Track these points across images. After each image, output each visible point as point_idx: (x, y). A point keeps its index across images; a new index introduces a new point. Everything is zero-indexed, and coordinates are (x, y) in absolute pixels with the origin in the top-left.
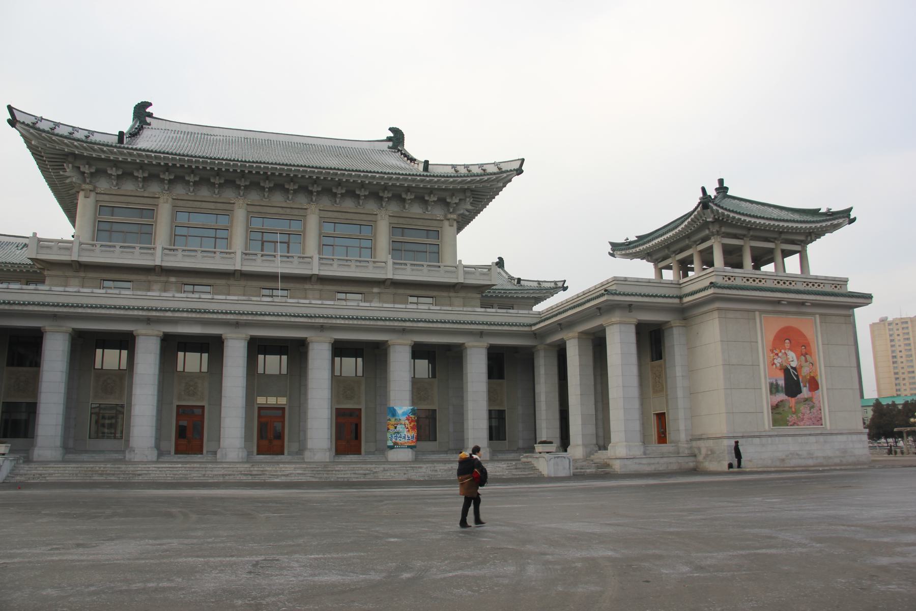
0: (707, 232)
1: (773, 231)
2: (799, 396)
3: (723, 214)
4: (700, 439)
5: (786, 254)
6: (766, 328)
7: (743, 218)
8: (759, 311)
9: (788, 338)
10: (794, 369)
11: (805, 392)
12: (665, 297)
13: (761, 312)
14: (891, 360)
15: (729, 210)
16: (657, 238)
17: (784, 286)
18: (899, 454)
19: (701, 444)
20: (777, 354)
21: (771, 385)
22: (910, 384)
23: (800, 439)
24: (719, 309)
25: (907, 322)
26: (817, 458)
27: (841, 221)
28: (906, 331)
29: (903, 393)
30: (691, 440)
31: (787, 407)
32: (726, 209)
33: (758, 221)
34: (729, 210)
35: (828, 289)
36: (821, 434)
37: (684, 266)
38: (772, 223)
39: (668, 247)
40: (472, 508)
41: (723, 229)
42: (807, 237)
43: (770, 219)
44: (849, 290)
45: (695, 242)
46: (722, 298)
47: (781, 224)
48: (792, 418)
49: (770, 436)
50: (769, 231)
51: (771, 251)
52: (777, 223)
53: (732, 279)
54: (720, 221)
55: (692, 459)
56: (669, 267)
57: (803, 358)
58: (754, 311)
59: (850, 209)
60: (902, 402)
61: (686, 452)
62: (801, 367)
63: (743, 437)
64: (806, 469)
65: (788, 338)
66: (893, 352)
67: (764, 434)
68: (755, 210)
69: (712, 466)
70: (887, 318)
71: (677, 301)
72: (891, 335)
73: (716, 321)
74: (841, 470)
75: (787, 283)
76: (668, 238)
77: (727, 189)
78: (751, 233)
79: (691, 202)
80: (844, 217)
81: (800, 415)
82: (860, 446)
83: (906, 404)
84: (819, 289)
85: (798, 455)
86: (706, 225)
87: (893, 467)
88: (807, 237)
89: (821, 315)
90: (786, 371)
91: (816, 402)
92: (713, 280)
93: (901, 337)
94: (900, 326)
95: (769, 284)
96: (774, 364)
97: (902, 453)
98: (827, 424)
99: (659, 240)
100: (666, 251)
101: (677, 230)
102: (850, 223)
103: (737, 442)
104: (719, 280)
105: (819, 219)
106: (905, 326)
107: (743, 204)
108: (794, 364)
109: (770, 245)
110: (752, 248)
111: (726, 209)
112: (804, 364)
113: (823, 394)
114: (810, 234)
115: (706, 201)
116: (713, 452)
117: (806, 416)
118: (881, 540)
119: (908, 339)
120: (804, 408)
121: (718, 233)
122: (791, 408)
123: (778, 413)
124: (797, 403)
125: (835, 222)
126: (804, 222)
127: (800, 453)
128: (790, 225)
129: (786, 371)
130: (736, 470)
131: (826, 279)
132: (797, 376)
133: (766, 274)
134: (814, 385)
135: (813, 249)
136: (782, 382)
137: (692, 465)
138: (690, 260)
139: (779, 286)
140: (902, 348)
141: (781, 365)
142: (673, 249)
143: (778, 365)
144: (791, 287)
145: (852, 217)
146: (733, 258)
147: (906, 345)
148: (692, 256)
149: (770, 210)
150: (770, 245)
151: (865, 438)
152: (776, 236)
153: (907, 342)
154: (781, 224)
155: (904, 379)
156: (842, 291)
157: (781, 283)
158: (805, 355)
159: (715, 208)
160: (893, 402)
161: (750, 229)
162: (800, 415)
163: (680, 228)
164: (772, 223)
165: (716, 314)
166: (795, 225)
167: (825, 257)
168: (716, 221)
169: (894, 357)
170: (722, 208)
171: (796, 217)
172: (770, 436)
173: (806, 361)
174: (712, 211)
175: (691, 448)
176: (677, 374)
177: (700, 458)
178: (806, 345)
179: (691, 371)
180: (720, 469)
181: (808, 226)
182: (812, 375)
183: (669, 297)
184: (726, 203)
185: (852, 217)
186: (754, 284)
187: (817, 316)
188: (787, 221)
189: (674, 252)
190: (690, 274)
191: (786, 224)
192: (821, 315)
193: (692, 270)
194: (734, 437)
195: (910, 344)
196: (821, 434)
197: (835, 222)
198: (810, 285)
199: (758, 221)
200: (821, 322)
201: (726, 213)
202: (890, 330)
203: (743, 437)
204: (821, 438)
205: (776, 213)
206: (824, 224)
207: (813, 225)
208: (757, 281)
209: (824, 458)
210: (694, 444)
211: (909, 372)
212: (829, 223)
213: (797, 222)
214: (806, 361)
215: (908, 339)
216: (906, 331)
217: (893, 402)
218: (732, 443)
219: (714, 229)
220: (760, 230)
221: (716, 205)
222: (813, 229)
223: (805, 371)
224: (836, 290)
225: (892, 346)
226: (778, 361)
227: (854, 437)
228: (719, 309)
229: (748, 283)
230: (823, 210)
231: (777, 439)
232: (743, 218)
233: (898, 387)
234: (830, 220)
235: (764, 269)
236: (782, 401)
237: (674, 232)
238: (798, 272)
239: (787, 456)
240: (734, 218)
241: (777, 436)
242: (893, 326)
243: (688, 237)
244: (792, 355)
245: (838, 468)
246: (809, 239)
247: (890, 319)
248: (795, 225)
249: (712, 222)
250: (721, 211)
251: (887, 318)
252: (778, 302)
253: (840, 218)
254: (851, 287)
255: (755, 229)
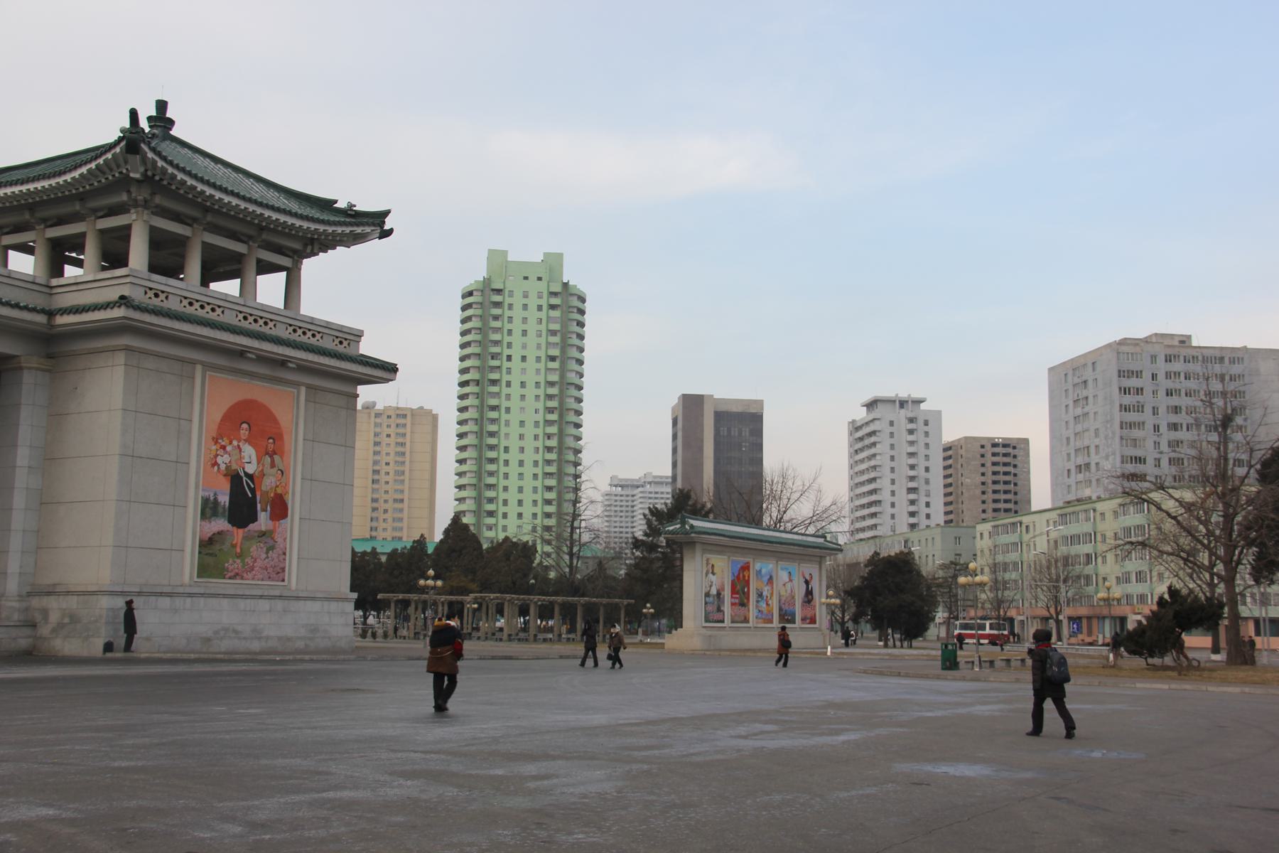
0: (124, 197)
1: (251, 223)
2: (251, 526)
3: (164, 171)
4: (49, 594)
5: (266, 268)
6: (212, 396)
7: (200, 187)
8: (202, 363)
9: (246, 420)
10: (250, 477)
11: (263, 520)
12: (17, 306)
13: (207, 367)
14: (370, 477)
15: (177, 167)
16: (16, 183)
17: (255, 327)
18: (369, 638)
19: (53, 603)
20: (224, 448)
21: (206, 501)
22: (394, 520)
23: (242, 603)
24: (127, 349)
25: (405, 416)
26: (268, 638)
27: (368, 229)
28: (401, 430)
29: (380, 534)
30: (29, 594)
31: (228, 544)
32: (171, 163)
33: (227, 199)
34: (177, 167)
35: (328, 344)
36: (280, 597)
37: (58, 255)
38: (251, 208)
39: (32, 207)
40: (1049, 705)
41: (158, 200)
42: (306, 245)
43: (250, 200)
44: (362, 351)
45: (94, 211)
46: (137, 330)
47: (267, 213)
48: (233, 565)
49: (191, 595)
50: (243, 221)
51: (239, 258)
52: (259, 210)
53: (162, 296)
54: (155, 182)
55: (27, 631)
56: (26, 249)
57: (268, 459)
58: (193, 363)
59: (387, 213)
60: (389, 550)
61: (16, 616)
62: (263, 475)
63: (140, 594)
64: (252, 657)
65: (246, 420)
66: (375, 463)
67: (181, 590)
68: (219, 173)
69: (68, 646)
70: (374, 404)
71: (41, 319)
72: (376, 435)
73: (119, 372)
74: (311, 661)
75: (261, 322)
76: (44, 190)
77: (171, 122)
78: (209, 218)
79: (108, 130)
80: (373, 224)
81: (248, 560)
82: (340, 620)
83: (393, 555)
84: (313, 341)
85: (235, 631)
86: (125, 182)
87: (393, 659)
88: (306, 245)
89: (309, 387)
90: (235, 479)
91: (279, 540)
92: (126, 291)
93: (392, 440)
94: (393, 422)
95: (229, 318)
96: (216, 464)
97: (374, 635)
98: (293, 580)
99: (16, 189)
100: (27, 216)
101: (61, 180)
102: (380, 238)
103: (129, 603)
104: (137, 295)
105: (332, 218)
106: (401, 421)
107: (200, 160)
108: (250, 469)
109: (240, 248)
110: (205, 246)
111: (171, 163)
112: (267, 470)
113: (293, 530)
114: (312, 241)
115: (132, 139)
116: (74, 619)
117: (259, 563)
118: (492, 772)
119: (403, 444)
120: (256, 550)
121: (146, 205)
122: (234, 546)
123: (211, 555)
124: (246, 538)
125: (359, 230)
126: (307, 218)
127: (239, 628)
128: (283, 218)
129: (235, 479)
130: (119, 655)
131: (328, 325)
132: (253, 491)
133: (225, 298)
134: (280, 509)
135: (311, 267)
136: (224, 499)
137: (23, 643)
138: (77, 243)
139: (245, 324)
140: (390, 459)
141: (227, 468)
142: (40, 214)
143: (223, 467)
144: (265, 330)
145: (387, 227)
146: (166, 259)
147: (397, 453)
148: (83, 235)
149: (249, 182)
150: (240, 248)
151: (352, 605)
152: (252, 232)
153: (400, 449)
154: (267, 213)
155: (386, 511)
156: (350, 351)
157: (251, 319)
158: (272, 454)
159: (150, 155)
160: (374, 549)
161: (207, 210)
162: (248, 560)
163: (68, 177)
164: (251, 208)
165: (121, 358)
166: (290, 220)
167: (331, 287)
168: (147, 180)
169: (376, 472)
170: (164, 159)
171: (294, 206)
172: (191, 595)
173: (273, 465)
174: (144, 159)
175: (27, 609)
176: (19, 463)
177: (45, 631)
178: (277, 437)
179: (49, 458)
180: (85, 653)
181: (313, 226)
182: (279, 491)
183: (26, 308)
184: (166, 148)
185: (387, 227)
186: (201, 313)
187: (303, 389)
188: (278, 210)
189: (44, 220)
190: (70, 271)
191: (275, 216)
192: (309, 387)
193: (79, 263)
194: (122, 593)
195: (403, 454)
196: (280, 597)
197: (359, 230)
198: (300, 332)
199: (227, 199)
200: (307, 400)
201: (170, 170)
202: (376, 425)
203: (140, 594)
204: (279, 604)
205: (258, 191)
206: (339, 229)
207: (321, 228)
208: (208, 308)
209: (280, 638)
210: (36, 602)
211: (395, 501)
212: (348, 230)
213: (296, 215)
214: (273, 465)
215: (403, 444)
216: (401, 430)
217: (374, 549)
218: (120, 603)
219: (141, 194)
220: (227, 215)
221: (153, 150)
222: (320, 234)
223: (268, 483)
224: (340, 349)
225: (376, 453)
226: (223, 460)
227: (334, 606)
228: (127, 349)
229: (190, 310)
230: (341, 205)
231: (202, 600)
232: (200, 187)
233: (374, 524)
234: (351, 224)
235: (214, 286)
236: (220, 533)
237: (53, 182)
238: (280, 304)
239: (216, 633)
240: (183, 183)
241: (202, 595)
242: (384, 419)
243: (82, 197)
244: (249, 451)
245: (307, 657)
246: (309, 249)
247: (379, 407)
248: (290, 220)
249: (137, 181)
250: (160, 163)
251: (374, 404)
252: (241, 354)
253: (368, 224)
254: (367, 348)
255: (218, 212)
